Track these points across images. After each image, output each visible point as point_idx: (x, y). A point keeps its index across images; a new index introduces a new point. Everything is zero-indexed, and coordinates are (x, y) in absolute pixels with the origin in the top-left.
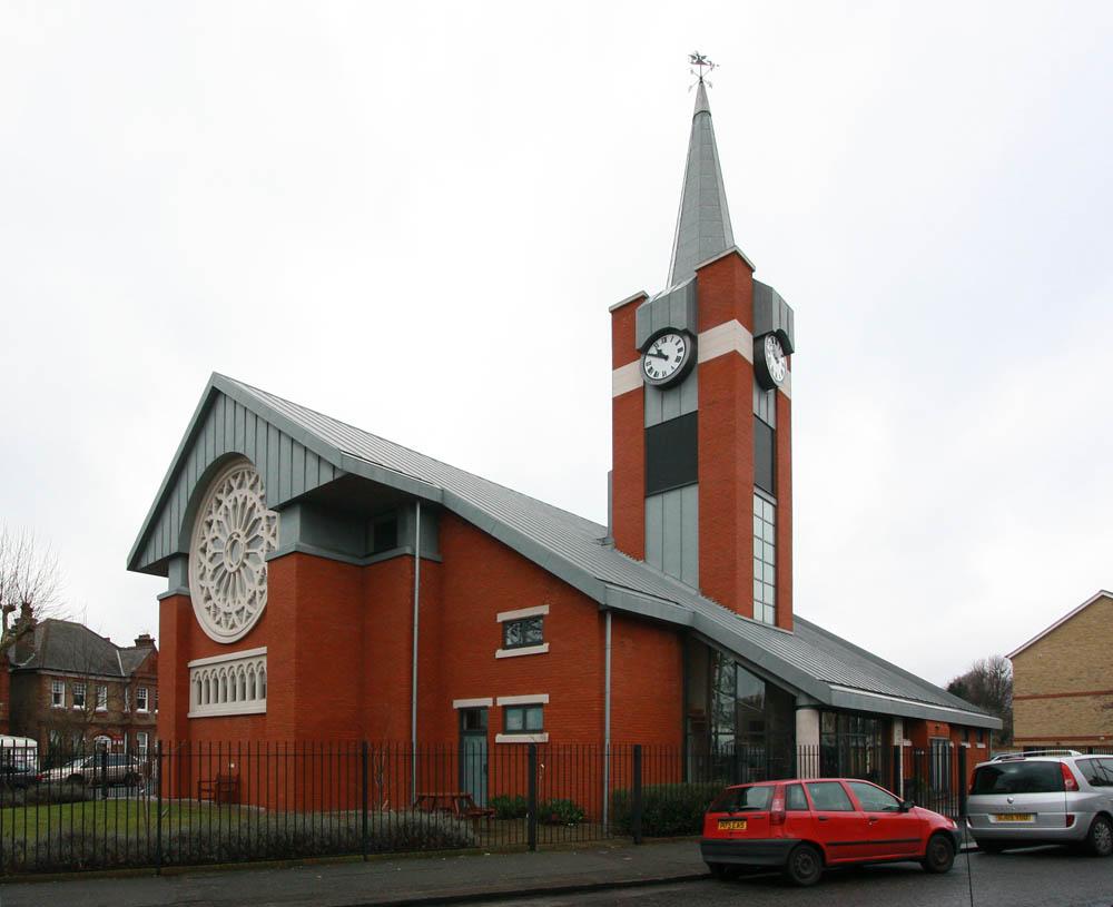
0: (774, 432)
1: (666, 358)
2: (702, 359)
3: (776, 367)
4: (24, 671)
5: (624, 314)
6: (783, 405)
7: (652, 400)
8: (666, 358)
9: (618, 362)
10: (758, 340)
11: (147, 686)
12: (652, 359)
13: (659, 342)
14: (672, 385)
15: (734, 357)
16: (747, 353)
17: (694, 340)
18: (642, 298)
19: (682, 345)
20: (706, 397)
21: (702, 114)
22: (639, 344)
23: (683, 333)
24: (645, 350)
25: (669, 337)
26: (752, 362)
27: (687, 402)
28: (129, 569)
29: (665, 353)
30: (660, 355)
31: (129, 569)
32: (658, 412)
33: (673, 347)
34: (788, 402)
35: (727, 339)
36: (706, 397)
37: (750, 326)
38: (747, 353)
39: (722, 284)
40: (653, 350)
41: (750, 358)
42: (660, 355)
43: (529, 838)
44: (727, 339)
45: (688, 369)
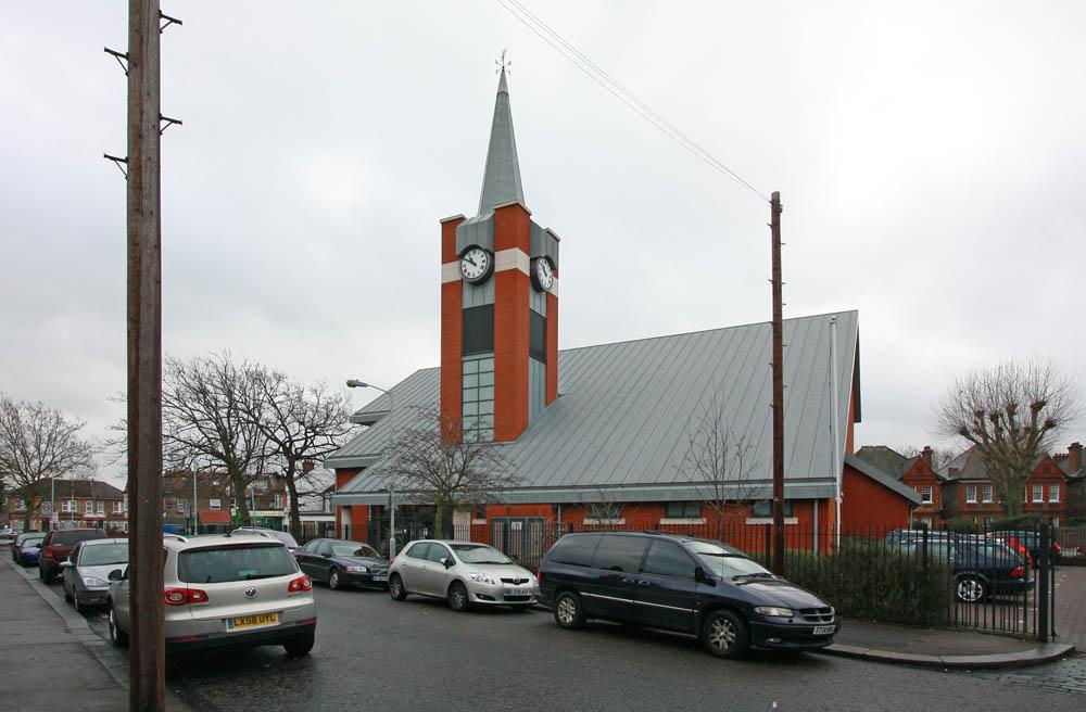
0: (545, 320)
1: (475, 265)
2: (496, 270)
3: (545, 280)
4: (1075, 480)
5: (450, 226)
6: (552, 301)
7: (467, 291)
8: (475, 265)
9: (445, 260)
10: (533, 260)
11: (931, 484)
12: (467, 263)
13: (471, 253)
14: (479, 283)
15: (515, 272)
16: (525, 269)
17: (492, 255)
18: (462, 219)
19: (484, 258)
20: (498, 289)
21: (503, 95)
22: (458, 252)
23: (486, 251)
24: (461, 257)
25: (477, 251)
26: (528, 274)
27: (487, 296)
28: (852, 316)
29: (475, 261)
30: (471, 261)
31: (852, 316)
32: (471, 299)
33: (479, 257)
34: (555, 299)
35: (514, 259)
36: (498, 289)
37: (527, 250)
38: (525, 269)
39: (509, 222)
40: (467, 257)
41: (527, 273)
42: (471, 261)
43: (1066, 558)
44: (514, 259)
45: (490, 272)
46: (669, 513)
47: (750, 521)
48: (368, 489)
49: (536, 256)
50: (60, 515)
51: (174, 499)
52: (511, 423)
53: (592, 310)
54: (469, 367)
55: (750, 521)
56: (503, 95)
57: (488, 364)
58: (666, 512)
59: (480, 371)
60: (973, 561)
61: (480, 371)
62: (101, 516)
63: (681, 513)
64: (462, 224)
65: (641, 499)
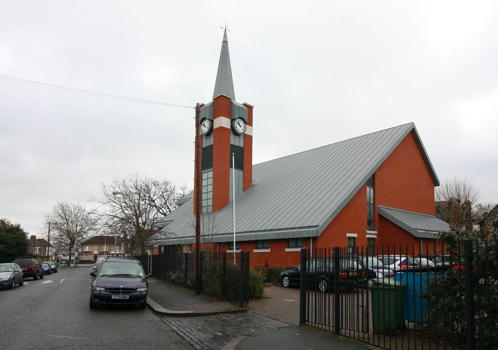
5: (199, 108)
6: (248, 139)
8: (241, 127)
10: (232, 121)
20: (222, 138)
21: (225, 42)
26: (230, 128)
30: (204, 125)
32: (207, 143)
36: (222, 138)
39: (223, 104)
42: (204, 125)
44: (223, 122)
45: (211, 130)
46: (290, 245)
47: (287, 250)
48: (190, 235)
49: (233, 118)
50: (97, 255)
51: (473, 230)
52: (222, 201)
53: (269, 144)
54: (204, 176)
55: (287, 250)
56: (225, 42)
57: (211, 174)
58: (256, 246)
59: (208, 176)
60: (327, 270)
61: (208, 176)
62: (117, 252)
63: (294, 245)
64: (204, 107)
65: (281, 237)
